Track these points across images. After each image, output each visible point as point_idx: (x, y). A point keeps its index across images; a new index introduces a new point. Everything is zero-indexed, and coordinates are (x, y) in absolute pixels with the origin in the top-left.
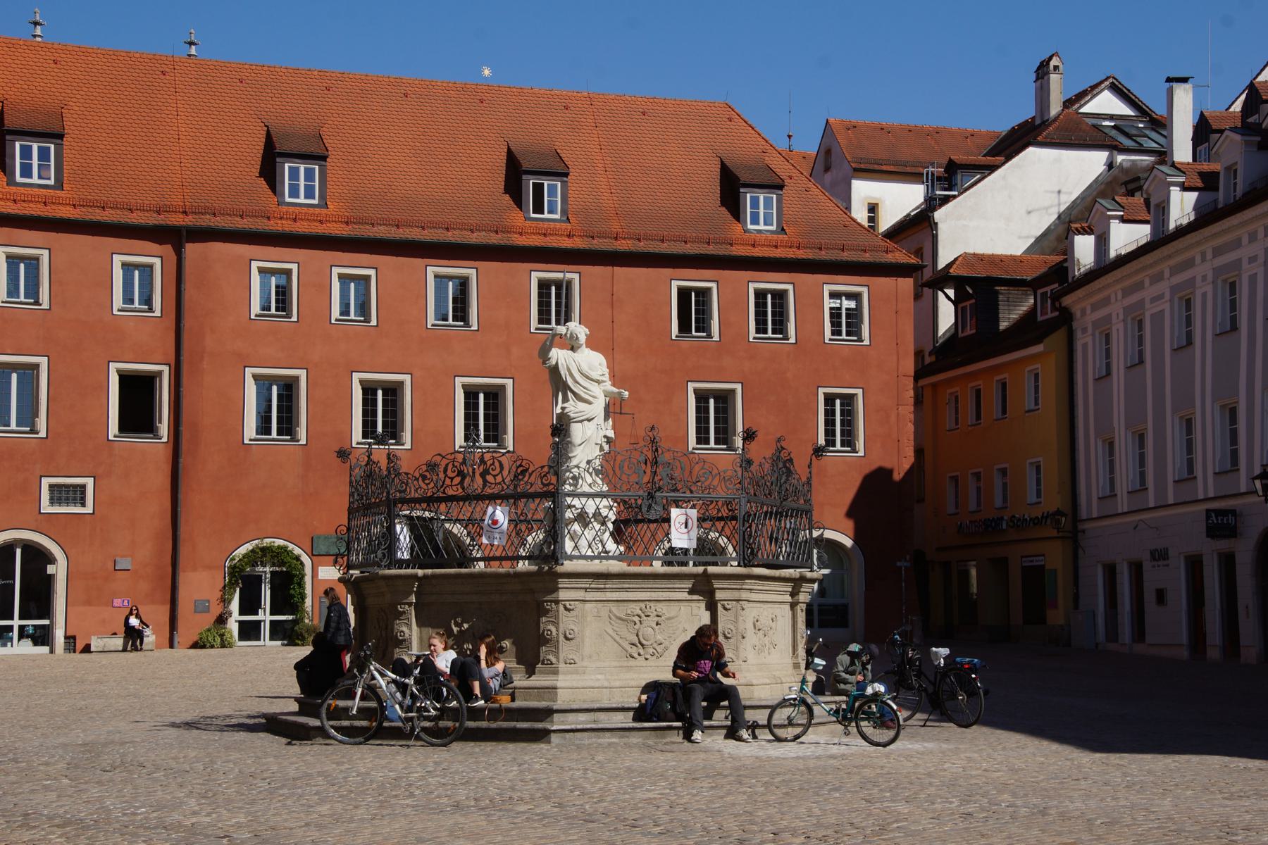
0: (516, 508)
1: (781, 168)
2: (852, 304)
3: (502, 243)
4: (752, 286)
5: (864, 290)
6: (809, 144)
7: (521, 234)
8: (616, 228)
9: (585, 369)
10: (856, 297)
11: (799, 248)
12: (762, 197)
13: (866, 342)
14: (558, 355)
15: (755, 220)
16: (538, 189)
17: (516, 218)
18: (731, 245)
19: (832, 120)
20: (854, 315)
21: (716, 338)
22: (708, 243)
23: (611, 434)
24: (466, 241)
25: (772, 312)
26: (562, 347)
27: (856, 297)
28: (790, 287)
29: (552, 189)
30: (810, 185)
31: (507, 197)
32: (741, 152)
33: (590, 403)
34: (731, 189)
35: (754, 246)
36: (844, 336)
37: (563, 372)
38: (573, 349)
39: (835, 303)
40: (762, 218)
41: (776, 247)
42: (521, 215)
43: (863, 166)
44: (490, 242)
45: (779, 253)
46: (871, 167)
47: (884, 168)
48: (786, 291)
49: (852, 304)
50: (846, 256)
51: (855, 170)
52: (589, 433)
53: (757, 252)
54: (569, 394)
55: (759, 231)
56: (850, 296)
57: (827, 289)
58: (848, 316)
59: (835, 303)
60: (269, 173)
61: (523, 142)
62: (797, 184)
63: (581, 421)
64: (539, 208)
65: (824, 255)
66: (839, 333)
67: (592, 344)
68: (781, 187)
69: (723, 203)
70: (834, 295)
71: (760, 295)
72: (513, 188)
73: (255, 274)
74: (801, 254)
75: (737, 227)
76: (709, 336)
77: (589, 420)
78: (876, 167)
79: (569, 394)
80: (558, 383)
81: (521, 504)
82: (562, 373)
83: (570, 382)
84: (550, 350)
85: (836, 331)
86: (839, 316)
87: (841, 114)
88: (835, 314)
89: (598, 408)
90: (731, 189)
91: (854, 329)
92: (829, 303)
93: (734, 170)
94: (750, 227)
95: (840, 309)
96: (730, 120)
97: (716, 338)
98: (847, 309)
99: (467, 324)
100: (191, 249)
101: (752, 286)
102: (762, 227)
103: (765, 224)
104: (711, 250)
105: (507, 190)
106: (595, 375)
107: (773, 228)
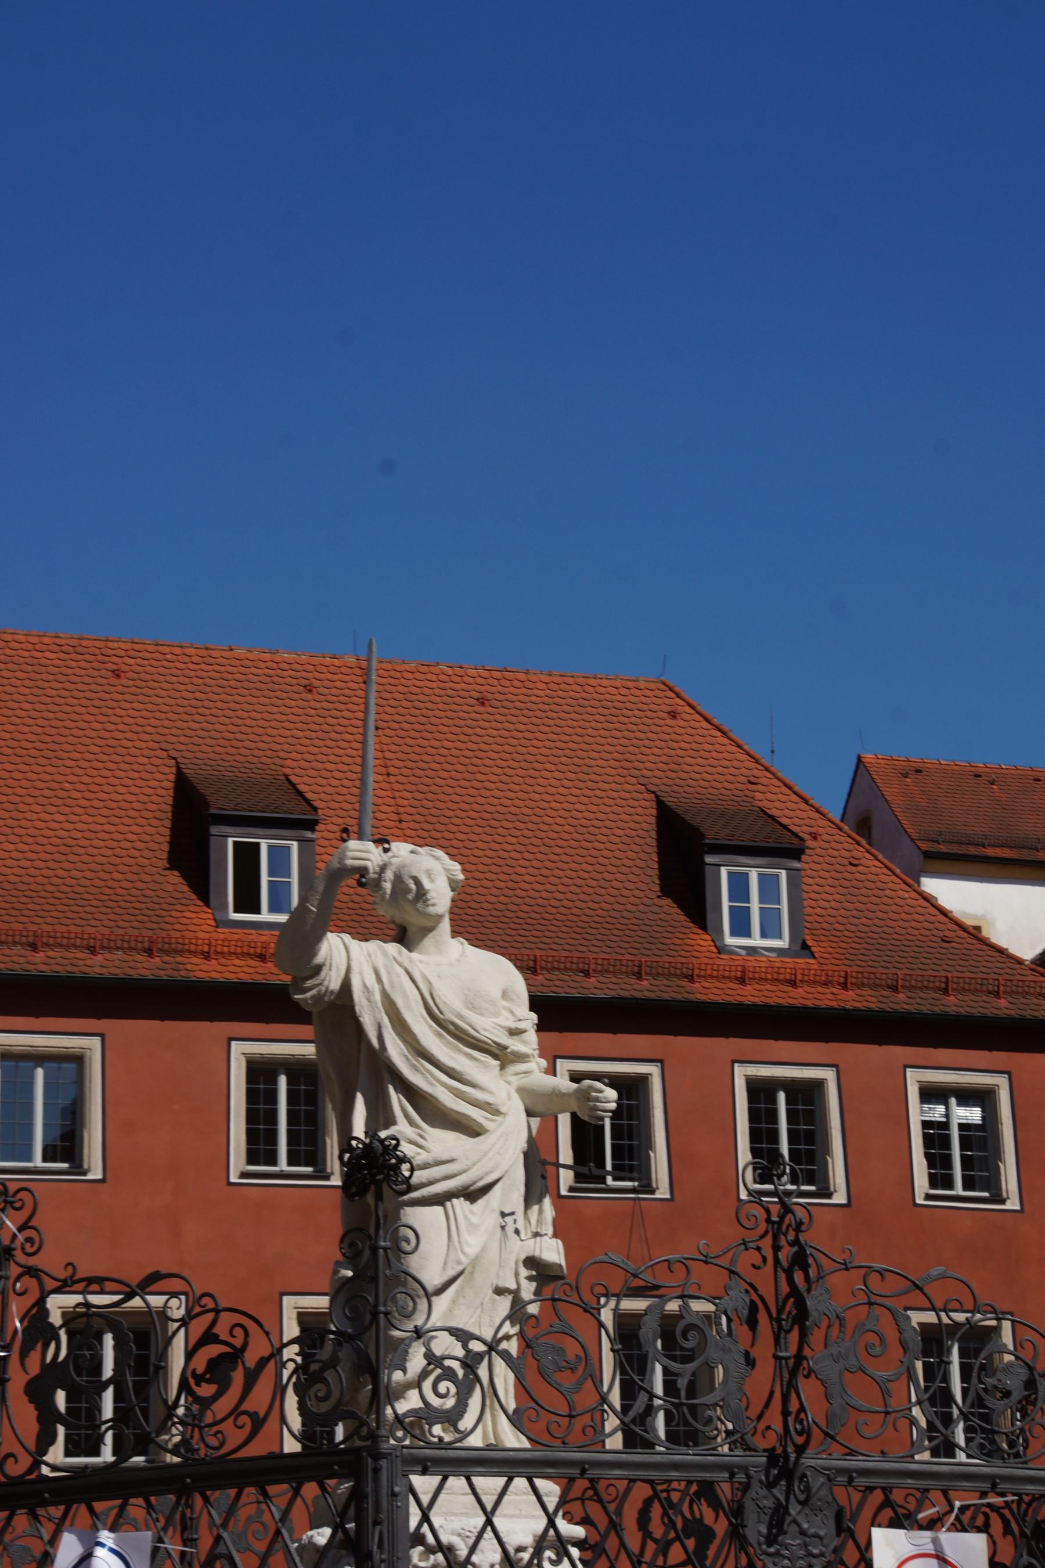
0: (187, 1530)
1: (795, 818)
2: (973, 1115)
3: (163, 975)
4: (741, 1073)
5: (1001, 1082)
6: (833, 800)
7: (207, 956)
9: (452, 1002)
10: (982, 1097)
11: (845, 986)
12: (754, 875)
13: (1013, 1204)
14: (347, 958)
15: (741, 927)
16: (247, 856)
17: (195, 922)
18: (691, 979)
19: (868, 757)
20: (981, 1141)
21: (663, 1192)
22: (639, 976)
23: (553, 1251)
24: (77, 971)
25: (791, 1134)
26: (364, 930)
27: (982, 1097)
28: (828, 1075)
29: (279, 857)
30: (859, 852)
31: (175, 878)
32: (703, 779)
33: (473, 1131)
35: (742, 981)
36: (959, 1190)
37: (370, 1016)
38: (404, 936)
39: (937, 1113)
40: (755, 922)
41: (793, 983)
42: (206, 915)
43: (942, 848)
44: (134, 974)
45: (800, 997)
46: (955, 849)
47: (990, 852)
48: (818, 1085)
49: (973, 1115)
50: (953, 1004)
51: (928, 856)
52: (472, 1244)
53: (750, 995)
54: (396, 1099)
55: (752, 950)
56: (967, 1096)
57: (914, 1079)
58: (965, 1143)
59: (937, 1113)
61: (210, 756)
62: (832, 848)
63: (440, 1200)
64: (248, 901)
65: (902, 1002)
66: (949, 1184)
67: (474, 923)
68: (796, 853)
69: (667, 889)
70: (931, 1094)
71: (761, 1093)
72: (190, 857)
74: (851, 999)
75: (702, 941)
76: (647, 1187)
77: (473, 1194)
78: (972, 850)
79: (396, 1099)
80: (349, 1057)
81: (207, 1512)
82: (367, 1021)
83: (396, 1051)
84: (318, 937)
85: (940, 1178)
86: (945, 1142)
87: (885, 747)
88: (936, 1136)
89: (501, 1150)
91: (982, 1171)
92: (918, 1113)
93: (687, 817)
94: (730, 940)
95: (945, 1125)
96: (673, 715)
97: (663, 1192)
98: (962, 1127)
99: (78, 1167)
101: (741, 1073)
102: (756, 941)
103: (764, 935)
104: (645, 989)
105: (175, 861)
106: (489, 1027)
107: (783, 943)
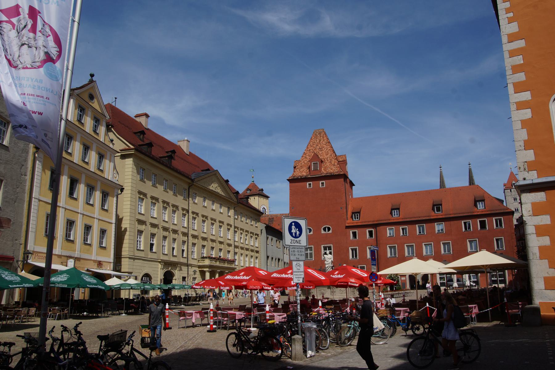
8: (451, 213)
17: (433, 213)
34: (476, 202)
60: (476, 205)
73: (389, 232)
90: (476, 202)
100: (378, 228)
